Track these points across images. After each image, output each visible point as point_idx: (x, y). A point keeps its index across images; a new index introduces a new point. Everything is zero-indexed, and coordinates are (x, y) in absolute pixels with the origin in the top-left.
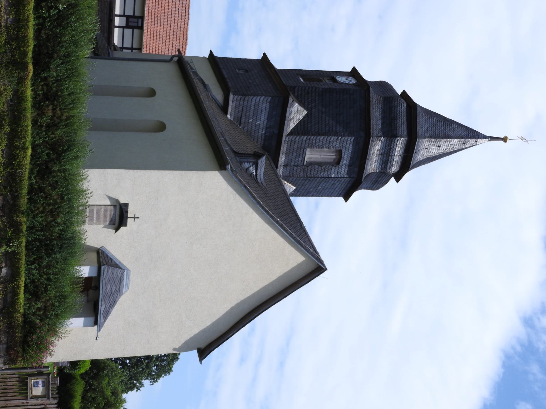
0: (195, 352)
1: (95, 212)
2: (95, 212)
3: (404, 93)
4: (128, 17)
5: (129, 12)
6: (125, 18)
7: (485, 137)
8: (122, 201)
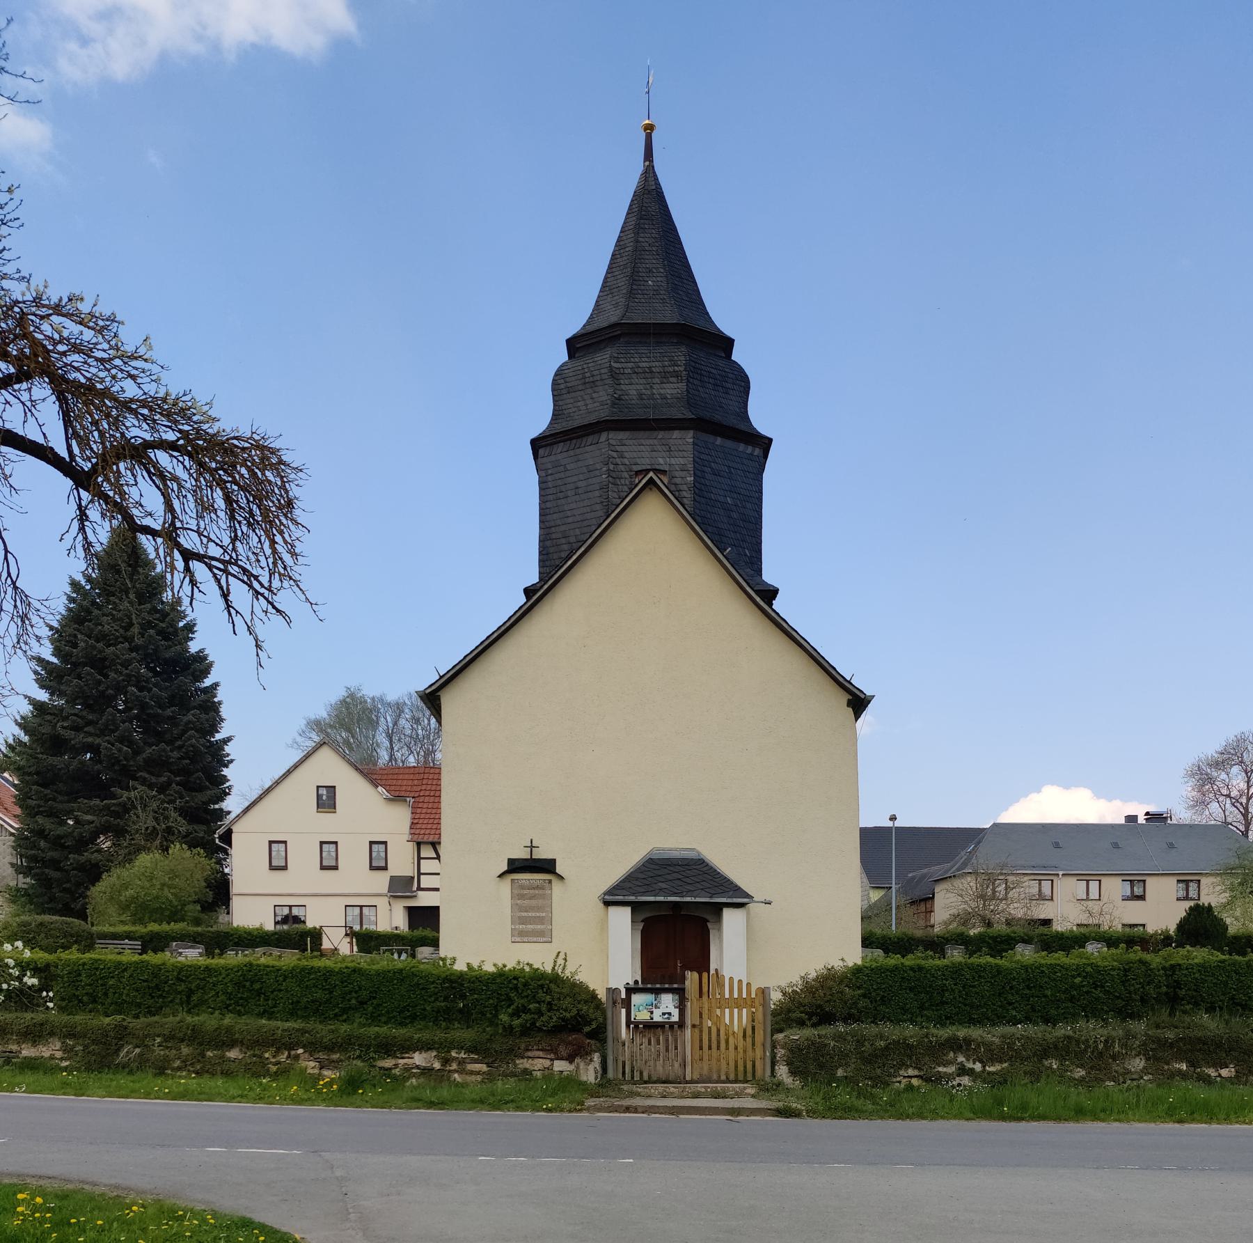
7: (649, 174)
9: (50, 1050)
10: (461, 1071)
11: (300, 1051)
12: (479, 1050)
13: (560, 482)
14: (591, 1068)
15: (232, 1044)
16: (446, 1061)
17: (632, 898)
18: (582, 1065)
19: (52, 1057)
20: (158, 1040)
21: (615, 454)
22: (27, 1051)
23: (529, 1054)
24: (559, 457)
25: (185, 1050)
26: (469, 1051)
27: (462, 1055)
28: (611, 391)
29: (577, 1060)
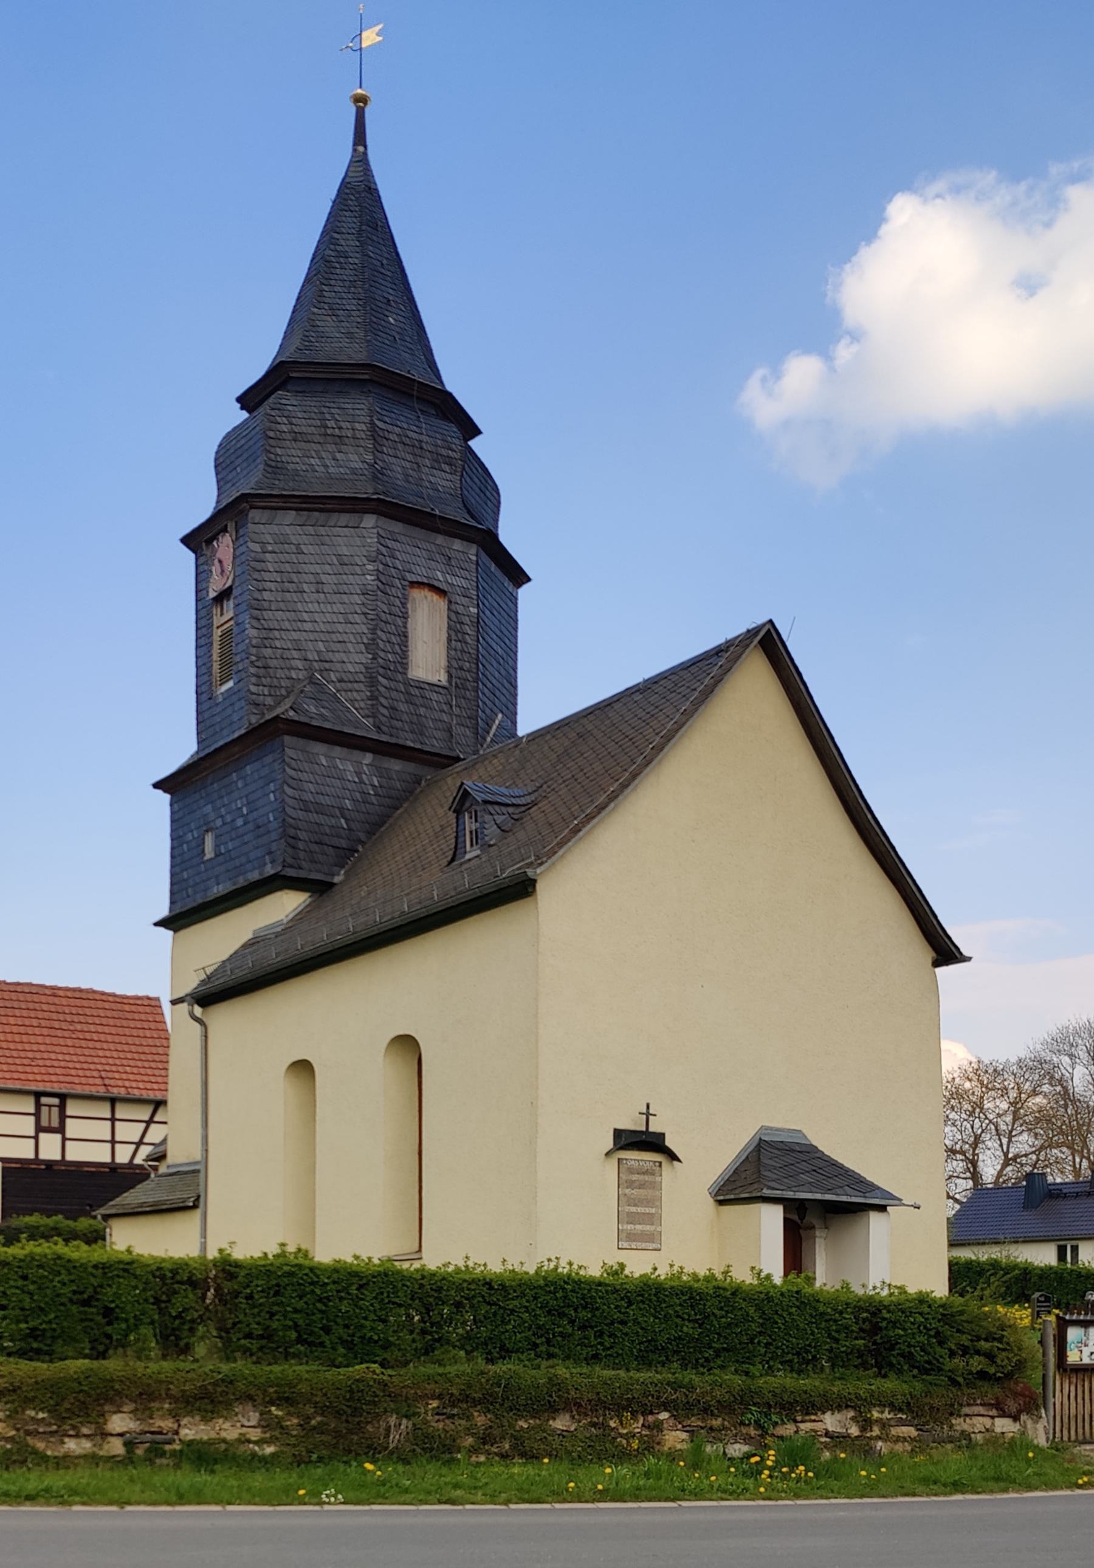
0: (941, 971)
1: (633, 1209)
2: (633, 1209)
3: (249, 400)
4: (39, 1129)
5: (27, 1125)
6: (42, 1136)
7: (360, 161)
8: (609, 1144)
9: (238, 1427)
10: (885, 1437)
11: (664, 1416)
12: (911, 1409)
13: (288, 567)
14: (1040, 1426)
15: (553, 1410)
16: (866, 1424)
17: (790, 1194)
18: (1029, 1424)
19: (244, 1440)
20: (435, 1404)
21: (383, 550)
22: (192, 1430)
23: (966, 1410)
24: (288, 530)
25: (480, 1420)
26: (894, 1408)
27: (887, 1415)
28: (369, 458)
29: (1024, 1417)
